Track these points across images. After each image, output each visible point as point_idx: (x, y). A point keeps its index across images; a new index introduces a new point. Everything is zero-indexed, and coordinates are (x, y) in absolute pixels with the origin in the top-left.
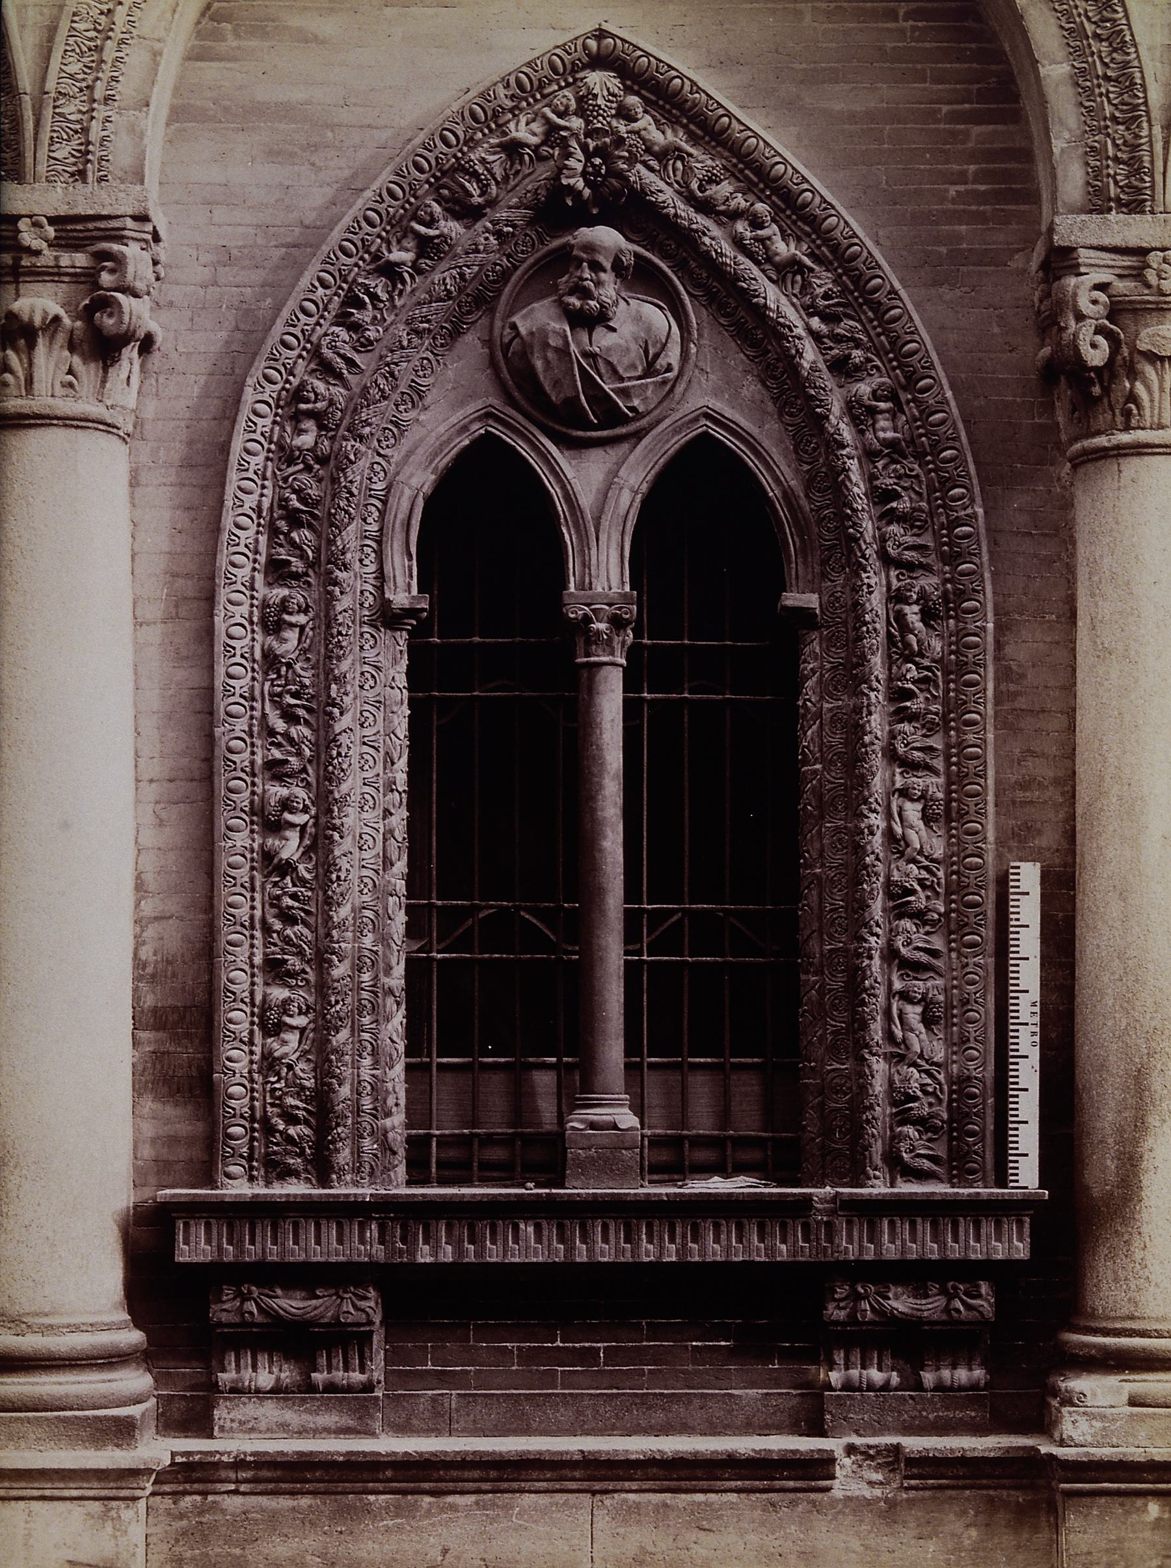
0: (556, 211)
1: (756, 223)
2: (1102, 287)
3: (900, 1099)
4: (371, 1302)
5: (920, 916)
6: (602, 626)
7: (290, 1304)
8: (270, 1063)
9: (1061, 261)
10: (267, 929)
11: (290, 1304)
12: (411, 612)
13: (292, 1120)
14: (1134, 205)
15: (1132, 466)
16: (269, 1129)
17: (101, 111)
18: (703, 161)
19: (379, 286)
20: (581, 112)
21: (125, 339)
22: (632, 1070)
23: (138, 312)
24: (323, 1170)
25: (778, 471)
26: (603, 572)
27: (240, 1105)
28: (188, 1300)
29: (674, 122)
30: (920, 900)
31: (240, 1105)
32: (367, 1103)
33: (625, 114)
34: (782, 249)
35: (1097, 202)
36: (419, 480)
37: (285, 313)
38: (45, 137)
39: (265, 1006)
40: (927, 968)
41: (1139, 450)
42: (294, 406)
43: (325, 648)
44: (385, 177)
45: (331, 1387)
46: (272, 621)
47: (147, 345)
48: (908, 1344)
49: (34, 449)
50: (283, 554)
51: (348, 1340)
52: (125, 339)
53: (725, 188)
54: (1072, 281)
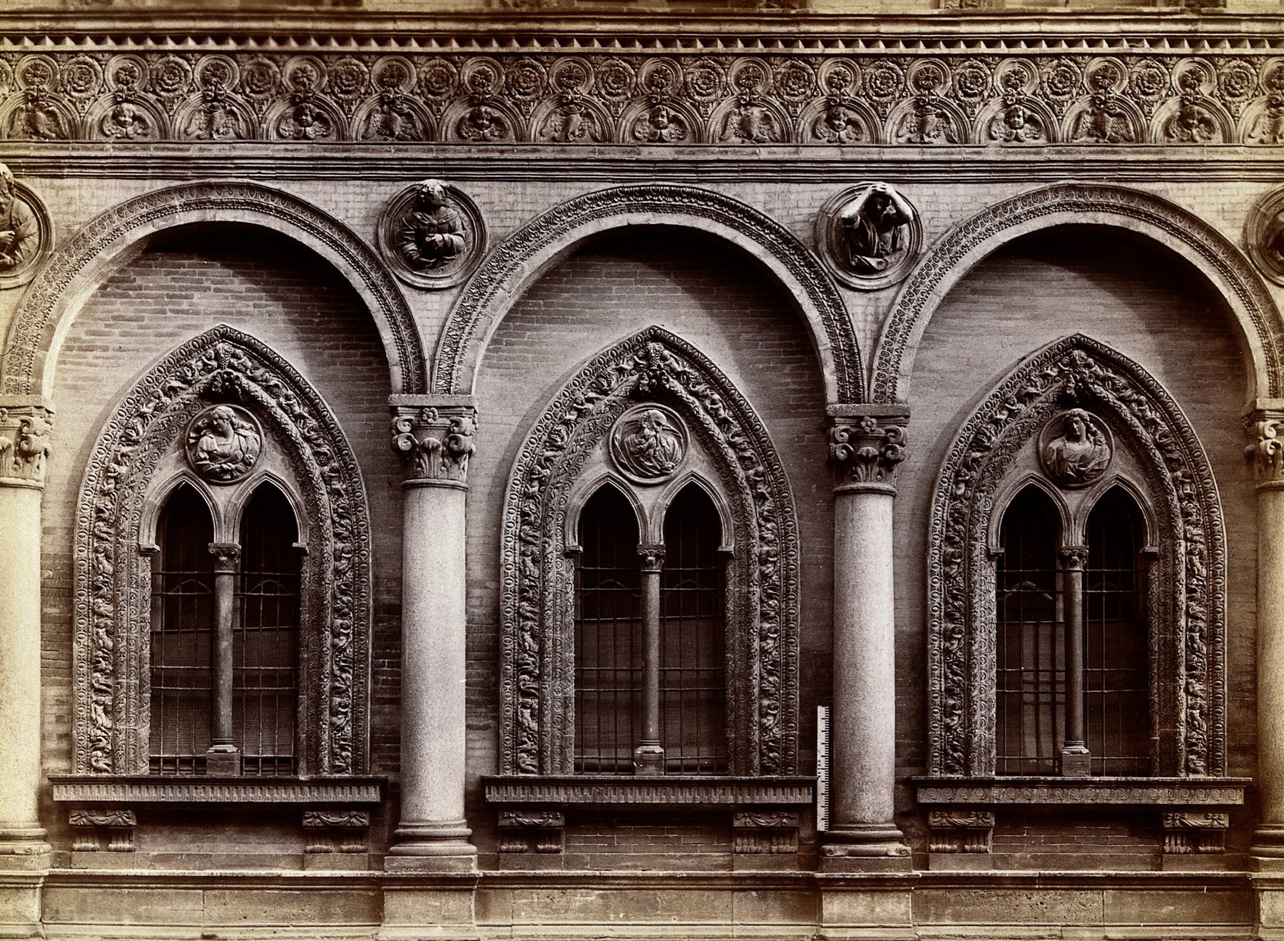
0: (1064, 400)
1: (1140, 403)
2: (1274, 426)
3: (1190, 745)
4: (992, 821)
5: (102, 671)
6: (224, 558)
7: (100, 819)
8: (948, 728)
9: (394, 411)
10: (946, 678)
11: (100, 819)
12: (996, 554)
13: (955, 750)
14: (422, 390)
15: (426, 491)
16: (946, 754)
17: (457, 366)
18: (1121, 381)
19: (562, 428)
20: (216, 359)
21: (461, 453)
22: (1085, 733)
23: (467, 443)
24: (967, 769)
25: (294, 496)
26: (226, 536)
27: (937, 745)
28: (59, 818)
29: (1107, 366)
30: (103, 664)
31: (937, 745)
32: (132, 740)
33: (1088, 366)
34: (297, 409)
35: (407, 389)
36: (1004, 503)
37: (98, 441)
38: (434, 378)
39: (945, 706)
40: (105, 692)
41: (422, 486)
42: (529, 475)
43: (968, 573)
44: (135, 384)
45: (972, 851)
46: (947, 561)
47: (470, 453)
48: (1195, 837)
49: (430, 495)
50: (951, 534)
51: (978, 834)
52: (461, 453)
53: (1129, 392)
54: (1261, 424)
